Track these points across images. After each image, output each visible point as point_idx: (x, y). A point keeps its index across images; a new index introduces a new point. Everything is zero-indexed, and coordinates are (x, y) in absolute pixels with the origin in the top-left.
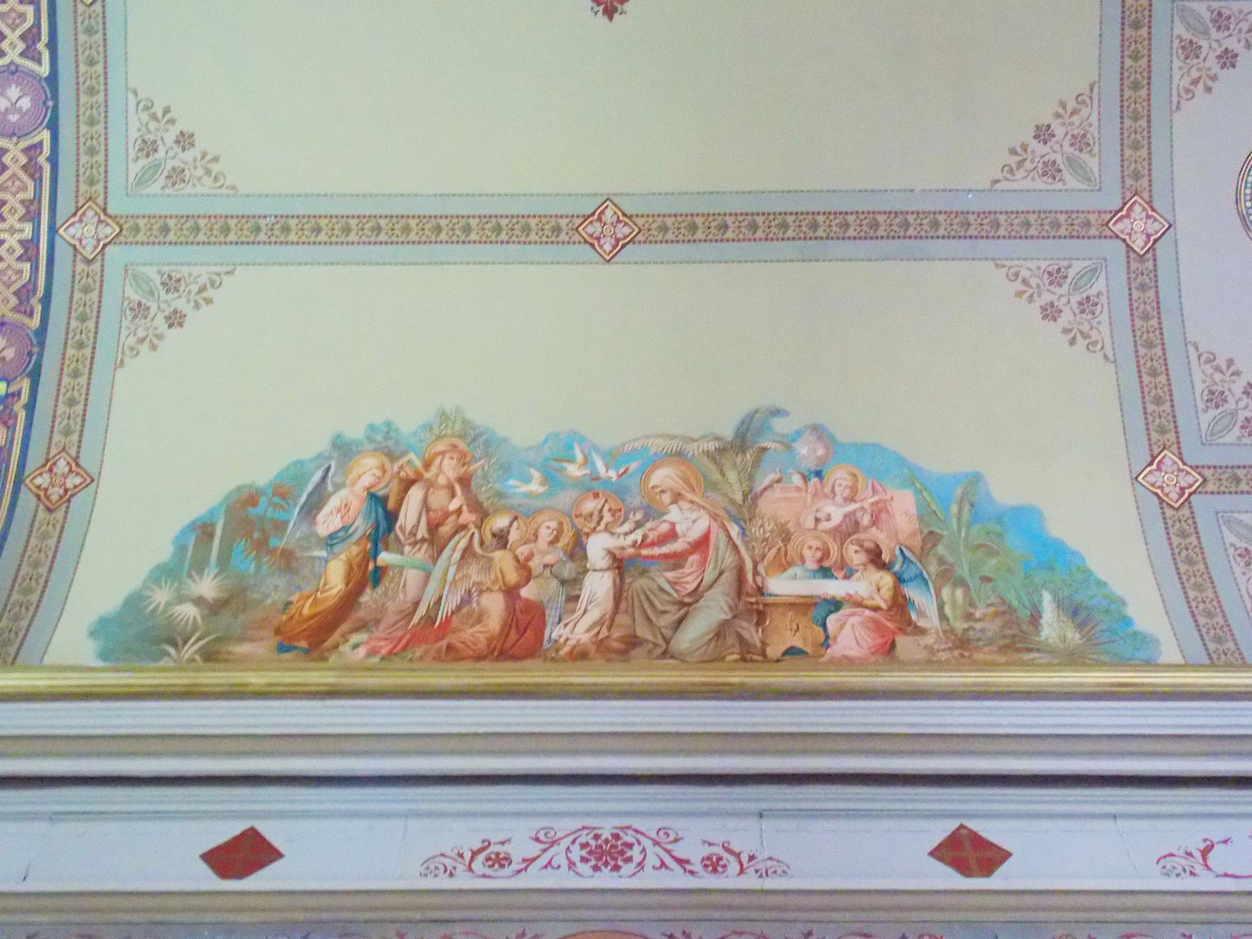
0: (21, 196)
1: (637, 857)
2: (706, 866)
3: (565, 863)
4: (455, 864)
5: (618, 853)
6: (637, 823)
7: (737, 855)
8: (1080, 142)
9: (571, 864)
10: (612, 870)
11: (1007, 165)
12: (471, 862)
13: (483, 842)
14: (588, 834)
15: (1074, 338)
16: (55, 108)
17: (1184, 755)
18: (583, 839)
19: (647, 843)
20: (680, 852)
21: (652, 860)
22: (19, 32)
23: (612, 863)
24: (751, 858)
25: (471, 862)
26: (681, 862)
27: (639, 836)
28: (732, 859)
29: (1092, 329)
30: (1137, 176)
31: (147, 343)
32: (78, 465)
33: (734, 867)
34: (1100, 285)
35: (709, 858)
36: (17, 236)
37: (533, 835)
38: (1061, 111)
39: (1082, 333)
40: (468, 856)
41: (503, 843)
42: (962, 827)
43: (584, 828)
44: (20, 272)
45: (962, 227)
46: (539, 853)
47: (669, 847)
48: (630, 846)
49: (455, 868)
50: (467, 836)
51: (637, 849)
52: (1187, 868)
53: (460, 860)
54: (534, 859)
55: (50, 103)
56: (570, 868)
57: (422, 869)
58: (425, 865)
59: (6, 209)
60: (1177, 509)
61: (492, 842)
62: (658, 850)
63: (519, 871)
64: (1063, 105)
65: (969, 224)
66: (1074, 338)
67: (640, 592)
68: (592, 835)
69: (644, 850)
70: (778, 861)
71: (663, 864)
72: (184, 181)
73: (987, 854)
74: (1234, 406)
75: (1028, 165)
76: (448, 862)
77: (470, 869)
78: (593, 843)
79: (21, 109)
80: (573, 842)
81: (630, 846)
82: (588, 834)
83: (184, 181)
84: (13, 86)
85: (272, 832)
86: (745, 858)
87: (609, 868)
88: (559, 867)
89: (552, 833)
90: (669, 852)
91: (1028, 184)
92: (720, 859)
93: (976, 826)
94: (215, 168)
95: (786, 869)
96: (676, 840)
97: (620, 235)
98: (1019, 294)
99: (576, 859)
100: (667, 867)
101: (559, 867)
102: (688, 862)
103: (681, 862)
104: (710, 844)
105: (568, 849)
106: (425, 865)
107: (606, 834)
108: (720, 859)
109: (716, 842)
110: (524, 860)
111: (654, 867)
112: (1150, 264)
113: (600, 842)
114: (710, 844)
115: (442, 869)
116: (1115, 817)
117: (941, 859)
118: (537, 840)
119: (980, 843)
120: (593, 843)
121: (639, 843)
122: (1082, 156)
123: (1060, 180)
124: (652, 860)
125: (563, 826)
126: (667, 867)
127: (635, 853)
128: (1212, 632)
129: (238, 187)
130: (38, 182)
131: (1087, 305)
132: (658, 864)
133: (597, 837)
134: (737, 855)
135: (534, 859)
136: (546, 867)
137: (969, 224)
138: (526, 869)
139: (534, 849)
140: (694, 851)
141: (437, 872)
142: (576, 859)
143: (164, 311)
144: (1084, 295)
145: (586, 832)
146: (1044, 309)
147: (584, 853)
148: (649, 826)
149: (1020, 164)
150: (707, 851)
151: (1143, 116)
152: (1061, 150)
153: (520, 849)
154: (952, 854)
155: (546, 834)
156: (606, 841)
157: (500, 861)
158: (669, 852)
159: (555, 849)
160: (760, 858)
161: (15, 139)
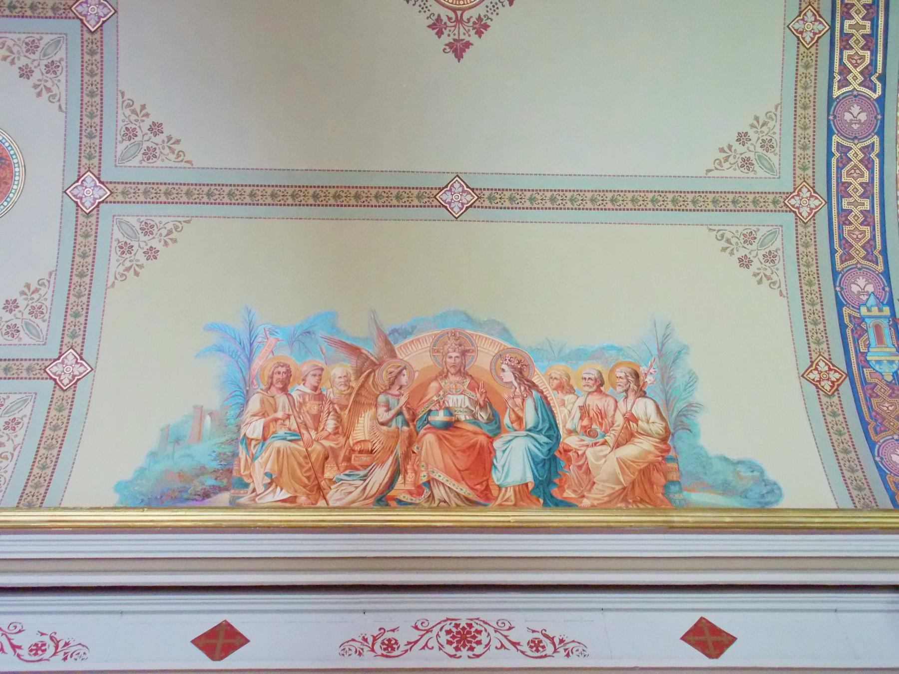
0: (860, 180)
1: (485, 640)
2: (531, 647)
3: (436, 645)
4: (362, 647)
5: (471, 637)
6: (483, 616)
7: (552, 639)
8: (767, 145)
9: (441, 647)
10: (468, 650)
11: (718, 159)
12: (373, 644)
13: (380, 629)
14: (450, 624)
15: (761, 279)
16: (883, 121)
17: (299, 571)
18: (447, 627)
19: (491, 630)
20: (513, 636)
21: (495, 643)
22: (859, 69)
23: (469, 645)
24: (561, 641)
25: (373, 644)
26: (515, 644)
27: (486, 626)
28: (548, 641)
29: (772, 273)
30: (90, 157)
31: (132, 271)
32: (82, 359)
33: (550, 649)
34: (778, 244)
35: (533, 641)
36: (860, 208)
37: (413, 625)
38: (755, 123)
39: (765, 275)
40: (370, 640)
41: (393, 630)
42: (702, 618)
43: (448, 619)
44: (863, 232)
45: (339, 195)
46: (418, 638)
47: (505, 633)
48: (479, 632)
49: (362, 649)
50: (369, 625)
51: (484, 634)
52: (358, 649)
53: (365, 644)
54: (416, 642)
55: (831, 118)
56: (440, 649)
57: (339, 650)
58: (342, 648)
59: (851, 188)
60: (64, 391)
61: (387, 629)
62: (498, 635)
63: (406, 651)
64: (757, 119)
65: (652, 201)
66: (761, 279)
67: (289, 452)
68: (453, 625)
69: (489, 635)
70: (579, 643)
71: (502, 645)
72: (156, 157)
73: (719, 638)
74: (20, 320)
75: (731, 160)
76: (357, 645)
77: (373, 650)
78: (454, 630)
79: (860, 120)
80: (441, 629)
81: (479, 632)
82: (450, 624)
83: (156, 157)
84: (855, 106)
85: (239, 623)
86: (557, 641)
87: (467, 648)
88: (433, 648)
89: (426, 623)
90: (506, 637)
91: (730, 173)
92: (540, 642)
93: (713, 618)
94: (177, 148)
95: (585, 649)
96: (510, 628)
97: (813, 206)
98: (724, 249)
99: (444, 642)
100: (505, 648)
101: (433, 648)
102: (519, 644)
103: (515, 644)
104: (533, 631)
105: (438, 635)
106: (342, 648)
107: (463, 624)
108: (540, 642)
109: (537, 630)
110: (409, 643)
111: (496, 648)
112: (811, 229)
113: (459, 629)
114: (533, 631)
115: (354, 650)
116: (122, 613)
117: (689, 642)
118: (416, 628)
119: (715, 630)
120: (454, 630)
121: (486, 630)
122: (769, 154)
123: (753, 171)
124: (495, 643)
125: (434, 618)
126: (505, 648)
127: (483, 637)
128: (854, 482)
129: (193, 162)
130: (871, 170)
131: (770, 257)
132: (499, 645)
133: (457, 626)
134: (552, 639)
135: (416, 642)
136: (423, 648)
137: (652, 201)
138: (411, 648)
139: (414, 635)
140: (522, 636)
141: (350, 652)
142: (444, 642)
143: (143, 248)
144: (767, 250)
145: (449, 622)
146: (740, 260)
147: (448, 637)
148: (492, 618)
149: (726, 159)
150: (532, 636)
151: (97, 116)
152: (752, 150)
153: (405, 635)
154: (697, 638)
155: (422, 623)
156: (464, 628)
157: (390, 645)
158: (506, 637)
159: (429, 635)
160: (72, 643)
161: (856, 141)
